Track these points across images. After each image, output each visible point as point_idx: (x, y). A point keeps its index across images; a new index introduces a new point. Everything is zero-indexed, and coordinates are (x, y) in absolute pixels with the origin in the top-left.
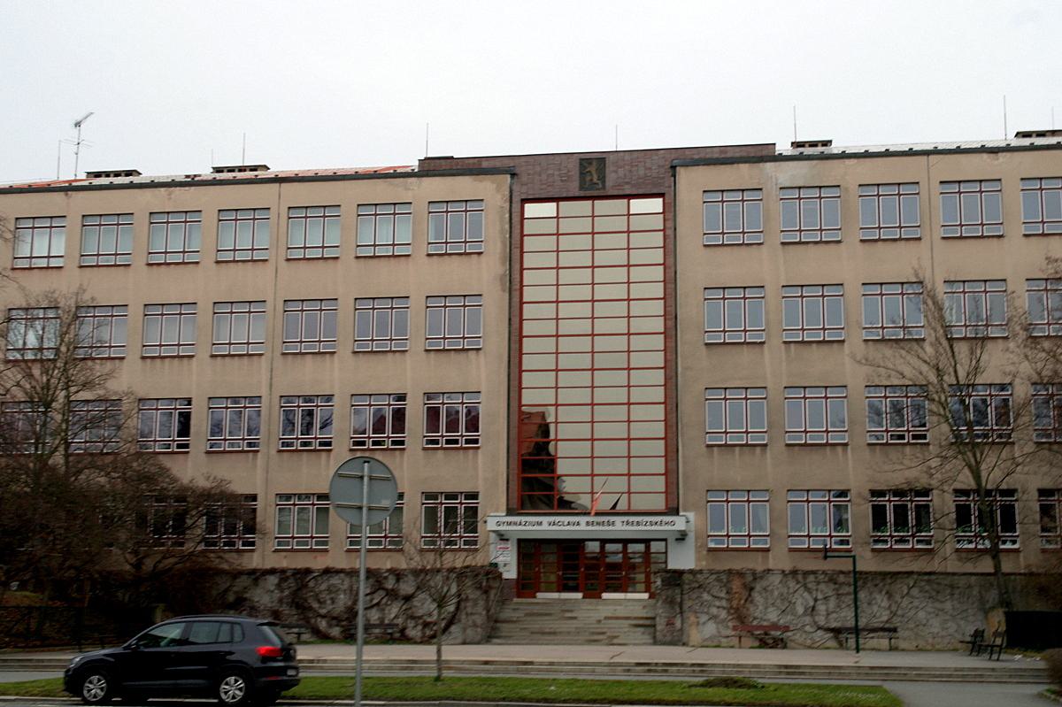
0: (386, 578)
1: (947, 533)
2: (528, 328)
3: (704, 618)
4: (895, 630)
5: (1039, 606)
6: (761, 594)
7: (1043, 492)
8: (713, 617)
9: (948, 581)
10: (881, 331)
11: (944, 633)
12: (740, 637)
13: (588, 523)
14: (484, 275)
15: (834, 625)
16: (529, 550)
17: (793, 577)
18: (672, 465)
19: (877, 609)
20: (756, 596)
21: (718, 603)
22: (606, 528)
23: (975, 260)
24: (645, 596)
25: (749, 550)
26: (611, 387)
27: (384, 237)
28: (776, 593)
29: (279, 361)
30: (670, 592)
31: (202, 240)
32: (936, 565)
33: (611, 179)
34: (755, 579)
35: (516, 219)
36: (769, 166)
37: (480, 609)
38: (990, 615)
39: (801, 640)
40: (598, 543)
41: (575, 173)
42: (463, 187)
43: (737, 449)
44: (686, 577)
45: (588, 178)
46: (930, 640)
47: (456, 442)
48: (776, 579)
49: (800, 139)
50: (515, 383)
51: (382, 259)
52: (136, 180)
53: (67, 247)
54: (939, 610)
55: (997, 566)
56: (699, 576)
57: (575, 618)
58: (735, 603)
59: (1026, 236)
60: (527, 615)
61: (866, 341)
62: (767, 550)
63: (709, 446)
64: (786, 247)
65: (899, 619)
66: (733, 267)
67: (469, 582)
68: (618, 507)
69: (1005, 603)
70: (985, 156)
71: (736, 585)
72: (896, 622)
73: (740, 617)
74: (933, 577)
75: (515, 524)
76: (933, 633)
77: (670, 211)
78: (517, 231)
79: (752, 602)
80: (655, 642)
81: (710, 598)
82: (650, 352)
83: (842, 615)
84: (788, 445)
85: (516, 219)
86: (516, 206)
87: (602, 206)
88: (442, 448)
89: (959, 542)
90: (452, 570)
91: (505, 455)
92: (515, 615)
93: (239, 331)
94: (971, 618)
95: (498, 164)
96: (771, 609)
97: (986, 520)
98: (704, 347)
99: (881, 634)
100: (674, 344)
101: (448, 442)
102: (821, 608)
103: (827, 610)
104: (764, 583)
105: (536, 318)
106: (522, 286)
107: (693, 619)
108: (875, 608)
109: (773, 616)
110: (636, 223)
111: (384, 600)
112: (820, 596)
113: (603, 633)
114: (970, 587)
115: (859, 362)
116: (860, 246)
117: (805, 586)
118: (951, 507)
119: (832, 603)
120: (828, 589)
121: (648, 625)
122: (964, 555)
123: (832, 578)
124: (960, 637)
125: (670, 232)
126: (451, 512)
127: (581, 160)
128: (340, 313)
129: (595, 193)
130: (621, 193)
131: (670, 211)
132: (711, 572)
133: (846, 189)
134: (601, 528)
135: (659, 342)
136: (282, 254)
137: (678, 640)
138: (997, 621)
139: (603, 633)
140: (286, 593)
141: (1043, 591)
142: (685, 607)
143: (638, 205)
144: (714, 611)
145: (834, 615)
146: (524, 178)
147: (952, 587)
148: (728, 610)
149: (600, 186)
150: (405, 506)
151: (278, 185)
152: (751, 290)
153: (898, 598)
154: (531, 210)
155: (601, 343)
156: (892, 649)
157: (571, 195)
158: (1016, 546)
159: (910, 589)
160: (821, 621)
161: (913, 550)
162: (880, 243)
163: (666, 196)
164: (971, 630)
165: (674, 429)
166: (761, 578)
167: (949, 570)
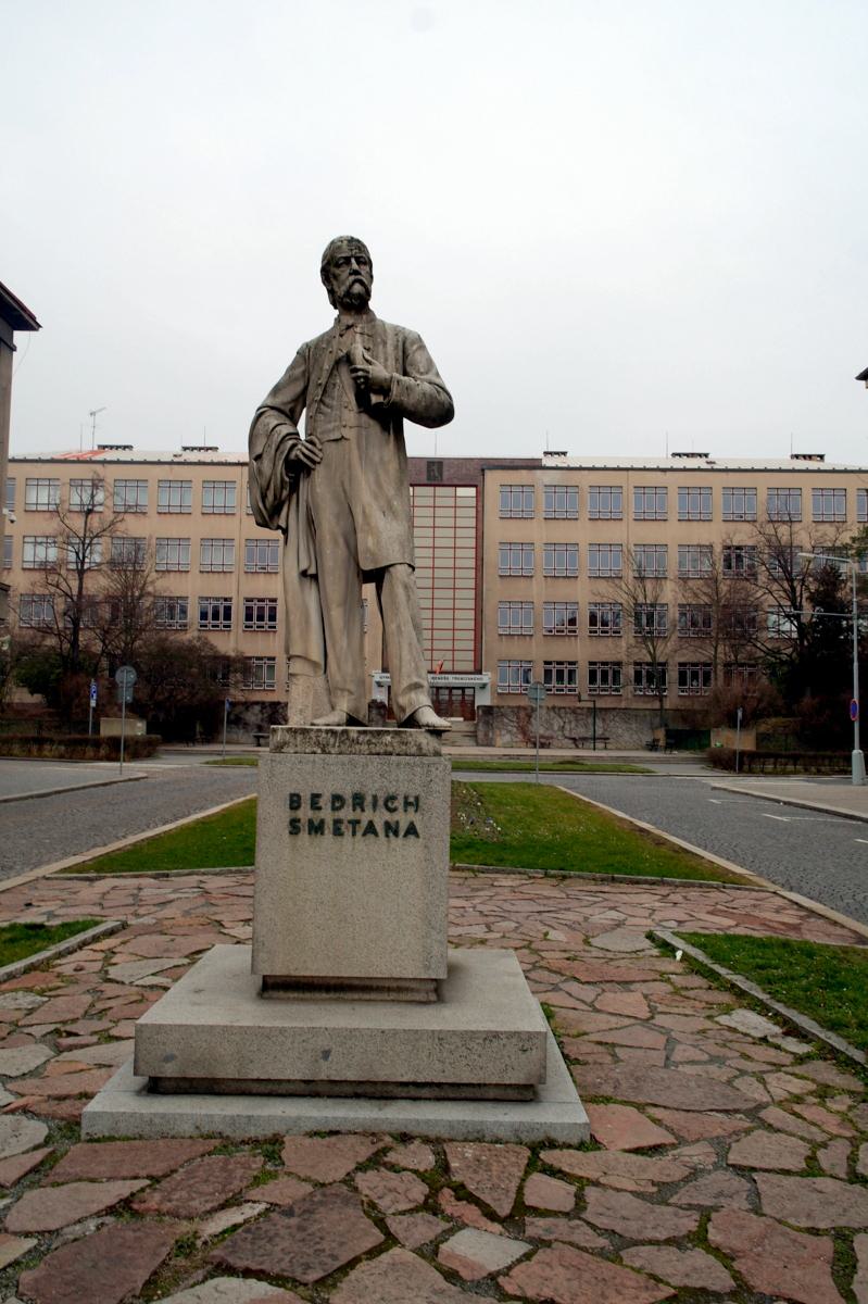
3: (504, 732)
5: (681, 726)
8: (509, 732)
9: (634, 713)
15: (573, 736)
23: (651, 533)
24: (462, 719)
26: (444, 598)
27: (219, 502)
29: (243, 576)
31: (193, 499)
33: (446, 474)
36: (539, 472)
41: (425, 469)
47: (218, 626)
52: (715, 467)
55: (450, 698)
63: (500, 635)
66: (516, 532)
70: (659, 473)
71: (522, 714)
72: (607, 735)
77: (480, 496)
80: (478, 744)
82: (467, 579)
87: (440, 491)
93: (217, 557)
97: (650, 680)
98: (498, 579)
102: (567, 727)
107: (498, 733)
116: (589, 523)
118: (632, 672)
119: (573, 725)
120: (572, 717)
121: (473, 735)
123: (574, 711)
125: (480, 509)
129: (436, 483)
131: (480, 496)
135: (472, 573)
137: (490, 744)
138: (661, 734)
140: (266, 715)
141: (684, 719)
143: (461, 491)
147: (636, 716)
152: (526, 546)
155: (438, 573)
156: (606, 748)
160: (567, 734)
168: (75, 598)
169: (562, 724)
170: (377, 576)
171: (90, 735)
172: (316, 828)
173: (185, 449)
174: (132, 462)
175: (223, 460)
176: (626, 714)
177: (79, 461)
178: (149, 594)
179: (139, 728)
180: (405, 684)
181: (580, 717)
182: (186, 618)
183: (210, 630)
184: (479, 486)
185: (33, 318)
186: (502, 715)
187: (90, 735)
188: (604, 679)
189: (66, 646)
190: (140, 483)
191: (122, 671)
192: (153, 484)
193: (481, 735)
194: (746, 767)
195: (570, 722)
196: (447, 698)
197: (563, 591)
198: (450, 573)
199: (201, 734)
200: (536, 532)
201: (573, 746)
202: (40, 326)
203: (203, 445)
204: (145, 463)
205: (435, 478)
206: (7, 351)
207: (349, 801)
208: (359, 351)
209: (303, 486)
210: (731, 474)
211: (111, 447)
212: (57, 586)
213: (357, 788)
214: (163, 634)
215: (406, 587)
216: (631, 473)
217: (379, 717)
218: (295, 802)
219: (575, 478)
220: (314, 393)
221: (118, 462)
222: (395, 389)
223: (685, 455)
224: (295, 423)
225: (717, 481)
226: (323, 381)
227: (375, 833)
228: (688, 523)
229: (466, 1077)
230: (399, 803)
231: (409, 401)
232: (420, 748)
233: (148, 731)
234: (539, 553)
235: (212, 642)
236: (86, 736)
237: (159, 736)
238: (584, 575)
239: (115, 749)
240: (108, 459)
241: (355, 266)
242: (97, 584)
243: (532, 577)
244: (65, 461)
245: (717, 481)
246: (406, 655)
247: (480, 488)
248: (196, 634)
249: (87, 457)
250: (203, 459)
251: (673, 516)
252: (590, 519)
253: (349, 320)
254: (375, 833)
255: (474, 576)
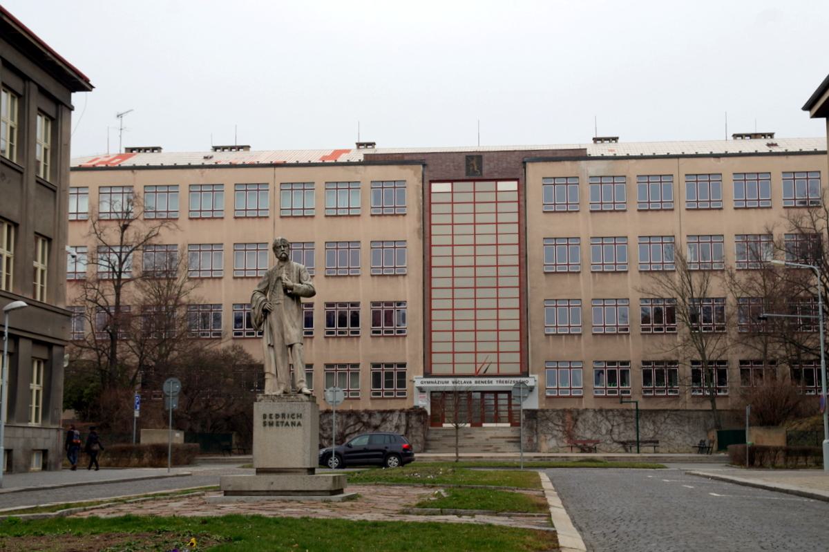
0: (363, 416)
1: (687, 388)
2: (435, 262)
3: (549, 437)
4: (657, 442)
6: (581, 422)
7: (742, 362)
8: (555, 436)
9: (687, 414)
10: (648, 204)
11: (684, 443)
12: (572, 447)
13: (476, 382)
14: (406, 228)
16: (438, 398)
17: (600, 413)
18: (524, 347)
19: (648, 431)
20: (579, 424)
21: (557, 429)
22: (487, 385)
23: (705, 223)
24: (509, 425)
25: (571, 397)
27: (343, 203)
28: (591, 422)
30: (530, 422)
32: (680, 406)
33: (485, 169)
34: (578, 414)
35: (426, 193)
36: (583, 163)
37: (420, 433)
38: (709, 433)
39: (604, 449)
40: (479, 394)
41: (463, 164)
42: (393, 172)
43: (564, 337)
44: (540, 414)
45: (471, 168)
46: (677, 448)
47: (392, 332)
48: (590, 414)
49: (599, 136)
50: (427, 296)
51: (342, 218)
53: (67, 178)
54: (681, 430)
56: (546, 413)
57: (473, 438)
58: (567, 428)
59: (735, 209)
60: (444, 436)
61: (640, 272)
62: (582, 397)
63: (546, 335)
64: (593, 214)
65: (659, 436)
66: (561, 226)
67: (414, 418)
68: (487, 372)
69: (717, 426)
70: (712, 159)
71: (568, 418)
72: (658, 438)
73: (570, 435)
74: (678, 413)
75: (432, 382)
76: (678, 444)
77: (522, 190)
78: (427, 201)
79: (577, 427)
81: (553, 425)
82: (511, 277)
83: (628, 434)
84: (594, 334)
85: (426, 193)
86: (426, 185)
87: (480, 186)
88: (383, 336)
89: (693, 391)
90: (402, 411)
91: (422, 340)
92: (437, 437)
94: (699, 436)
95: (415, 158)
96: (587, 431)
98: (543, 275)
99: (649, 444)
100: (525, 272)
101: (386, 332)
102: (616, 430)
103: (619, 432)
104: (583, 417)
105: (440, 256)
106: (431, 235)
107: (543, 437)
108: (646, 430)
109: (588, 435)
110: (501, 197)
111: (362, 429)
112: (615, 424)
113: (491, 446)
114: (699, 418)
115: (639, 291)
116: (637, 215)
117: (607, 418)
120: (619, 420)
121: (517, 441)
122: (696, 400)
123: (622, 413)
124: (692, 445)
125: (522, 203)
126: (389, 375)
127: (467, 156)
128: (316, 252)
130: (492, 178)
131: (522, 190)
132: (554, 411)
133: (630, 178)
134: (483, 385)
136: (278, 213)
138: (713, 435)
139: (491, 446)
142: (539, 431)
143: (502, 186)
144: (555, 433)
145: (623, 434)
146: (431, 168)
147: (689, 418)
148: (563, 432)
149: (479, 173)
150: (360, 372)
151: (273, 169)
152: (572, 241)
153: (659, 424)
154: (436, 187)
155: (480, 271)
157: (461, 178)
158: (727, 394)
159: (665, 419)
160: (616, 437)
161: (667, 396)
162: (649, 213)
163: (520, 181)
164: (698, 442)
165: (526, 324)
166: (582, 413)
167: (688, 408)
168: (112, 311)
169: (610, 428)
170: (291, 346)
171: (134, 444)
172: (271, 424)
173: (216, 148)
174: (162, 167)
175: (255, 161)
176: (679, 416)
177: (107, 168)
178: (182, 305)
179: (178, 437)
180: (299, 380)
181: (630, 419)
182: (219, 326)
183: (244, 338)
184: (521, 180)
185: (87, 81)
186: (547, 419)
187: (134, 444)
188: (660, 380)
189: (105, 359)
190: (171, 189)
191: (169, 383)
192: (184, 190)
193: (524, 440)
194: (757, 462)
195: (618, 425)
196: (493, 402)
197: (612, 287)
198: (492, 272)
199: (237, 444)
200: (582, 226)
201: (624, 451)
202: (92, 87)
203: (233, 144)
204: (175, 167)
205: (475, 172)
206: (67, 110)
207: (281, 416)
208: (284, 276)
209: (268, 317)
210: (791, 157)
211: (139, 150)
212: (95, 301)
213: (283, 412)
214: (198, 344)
215: (299, 350)
216: (682, 160)
217: (419, 424)
218: (265, 416)
219: (621, 167)
220: (271, 288)
221: (148, 168)
222: (295, 289)
223: (747, 135)
224: (266, 295)
225: (776, 167)
226: (273, 284)
227: (289, 425)
228: (745, 212)
229: (311, 489)
230: (295, 416)
231: (300, 292)
232: (302, 399)
233: (186, 441)
234: (586, 249)
235: (247, 351)
236: (130, 445)
237: (197, 445)
238: (634, 270)
239: (159, 456)
240: (138, 164)
241: (283, 249)
242: (134, 295)
243: (579, 272)
244: (93, 168)
245: (776, 167)
246: (299, 372)
247: (522, 182)
248: (230, 343)
249: (116, 163)
250: (234, 161)
251: (729, 204)
252: (639, 210)
253: (281, 264)
254: (289, 425)
255: (517, 274)
